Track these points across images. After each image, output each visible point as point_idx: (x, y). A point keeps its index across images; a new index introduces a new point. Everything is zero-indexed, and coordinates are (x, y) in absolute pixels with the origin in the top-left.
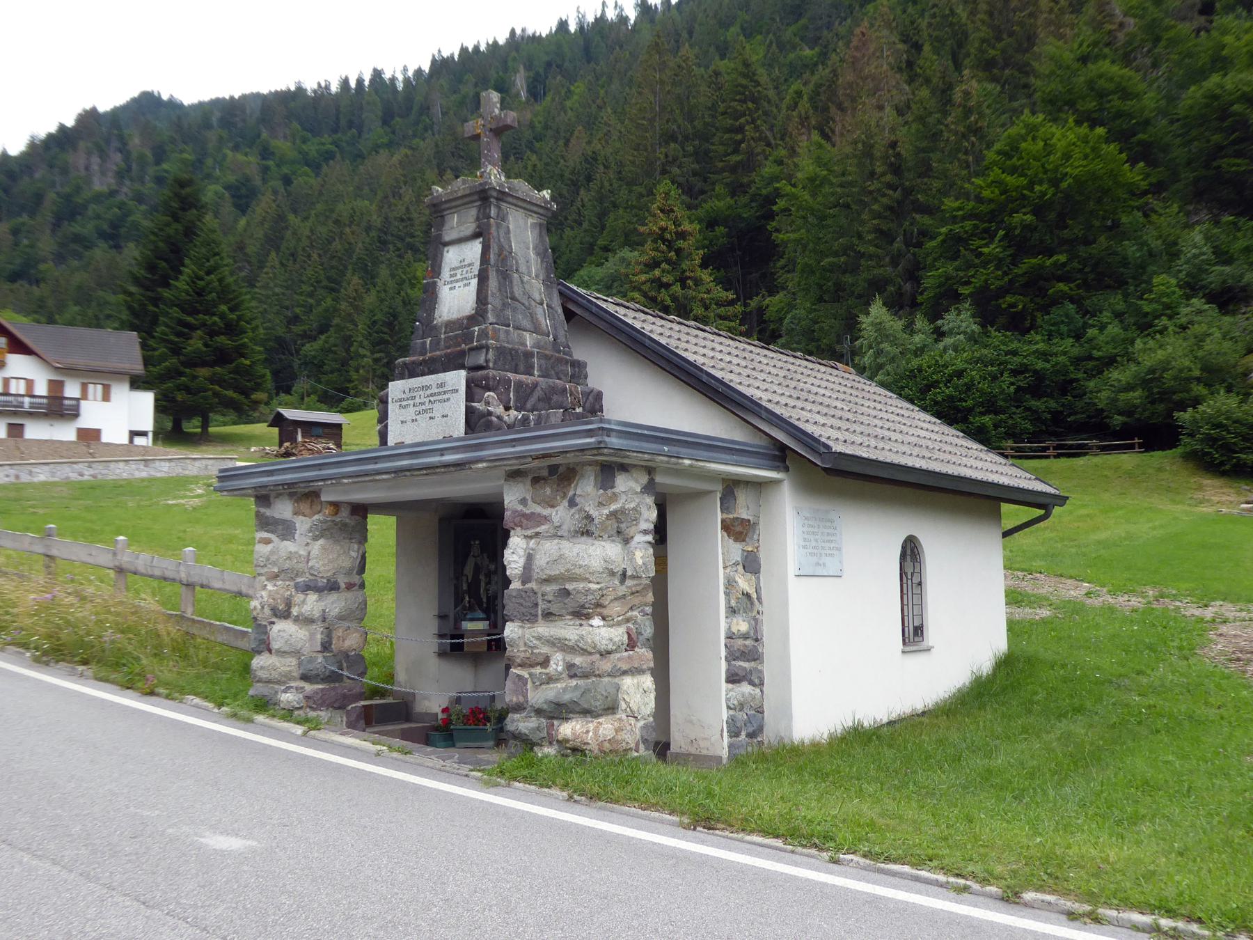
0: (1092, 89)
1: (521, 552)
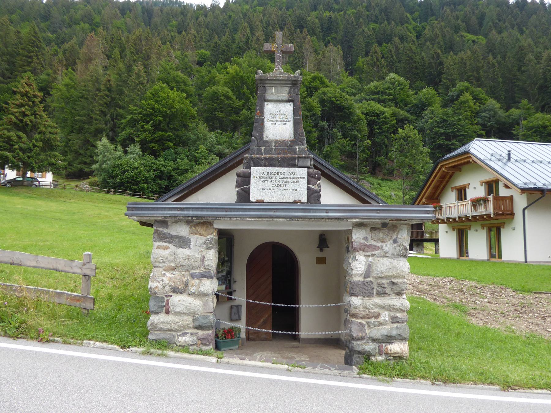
0: (175, 80)
1: (364, 263)
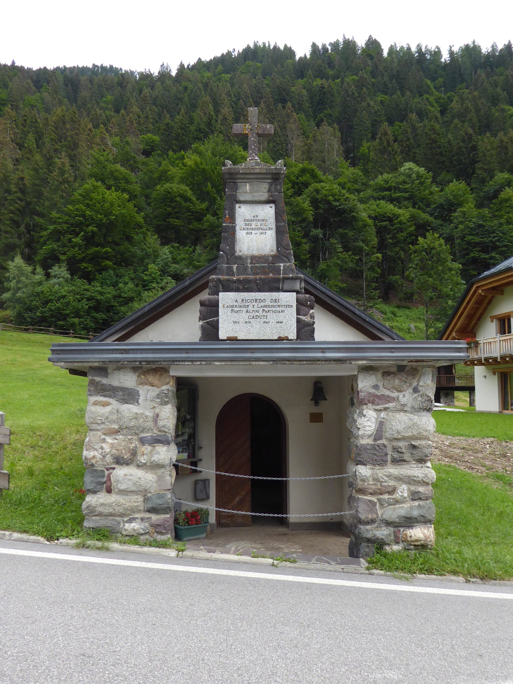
0: (112, 176)
1: (374, 420)
